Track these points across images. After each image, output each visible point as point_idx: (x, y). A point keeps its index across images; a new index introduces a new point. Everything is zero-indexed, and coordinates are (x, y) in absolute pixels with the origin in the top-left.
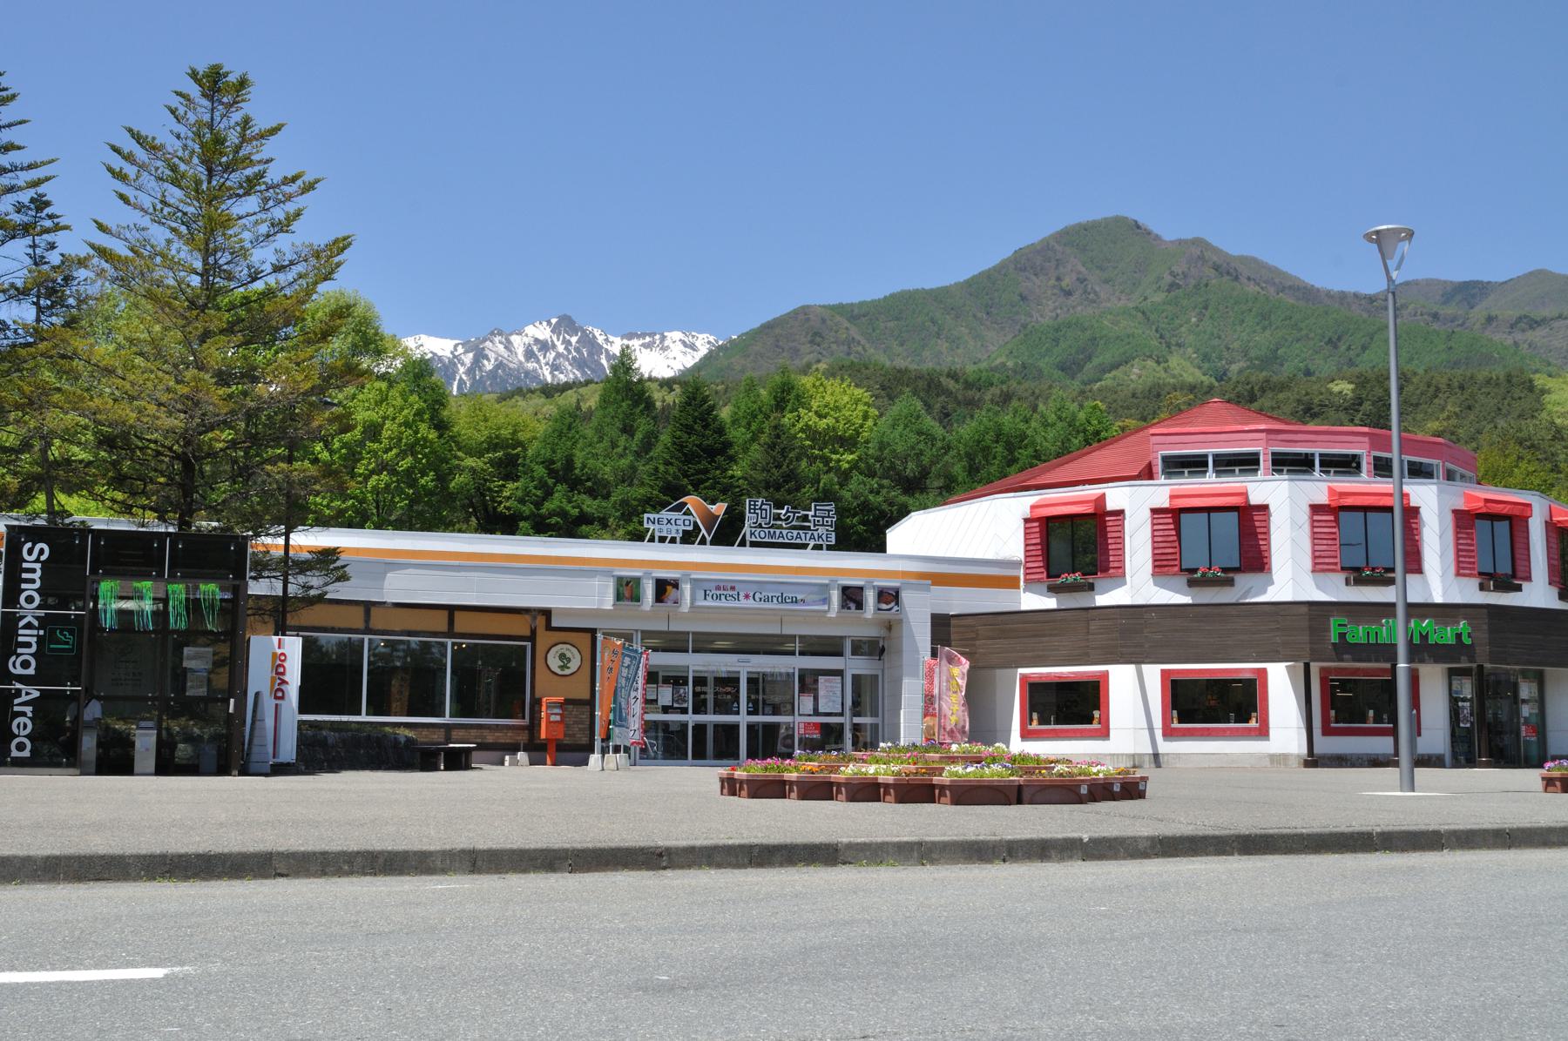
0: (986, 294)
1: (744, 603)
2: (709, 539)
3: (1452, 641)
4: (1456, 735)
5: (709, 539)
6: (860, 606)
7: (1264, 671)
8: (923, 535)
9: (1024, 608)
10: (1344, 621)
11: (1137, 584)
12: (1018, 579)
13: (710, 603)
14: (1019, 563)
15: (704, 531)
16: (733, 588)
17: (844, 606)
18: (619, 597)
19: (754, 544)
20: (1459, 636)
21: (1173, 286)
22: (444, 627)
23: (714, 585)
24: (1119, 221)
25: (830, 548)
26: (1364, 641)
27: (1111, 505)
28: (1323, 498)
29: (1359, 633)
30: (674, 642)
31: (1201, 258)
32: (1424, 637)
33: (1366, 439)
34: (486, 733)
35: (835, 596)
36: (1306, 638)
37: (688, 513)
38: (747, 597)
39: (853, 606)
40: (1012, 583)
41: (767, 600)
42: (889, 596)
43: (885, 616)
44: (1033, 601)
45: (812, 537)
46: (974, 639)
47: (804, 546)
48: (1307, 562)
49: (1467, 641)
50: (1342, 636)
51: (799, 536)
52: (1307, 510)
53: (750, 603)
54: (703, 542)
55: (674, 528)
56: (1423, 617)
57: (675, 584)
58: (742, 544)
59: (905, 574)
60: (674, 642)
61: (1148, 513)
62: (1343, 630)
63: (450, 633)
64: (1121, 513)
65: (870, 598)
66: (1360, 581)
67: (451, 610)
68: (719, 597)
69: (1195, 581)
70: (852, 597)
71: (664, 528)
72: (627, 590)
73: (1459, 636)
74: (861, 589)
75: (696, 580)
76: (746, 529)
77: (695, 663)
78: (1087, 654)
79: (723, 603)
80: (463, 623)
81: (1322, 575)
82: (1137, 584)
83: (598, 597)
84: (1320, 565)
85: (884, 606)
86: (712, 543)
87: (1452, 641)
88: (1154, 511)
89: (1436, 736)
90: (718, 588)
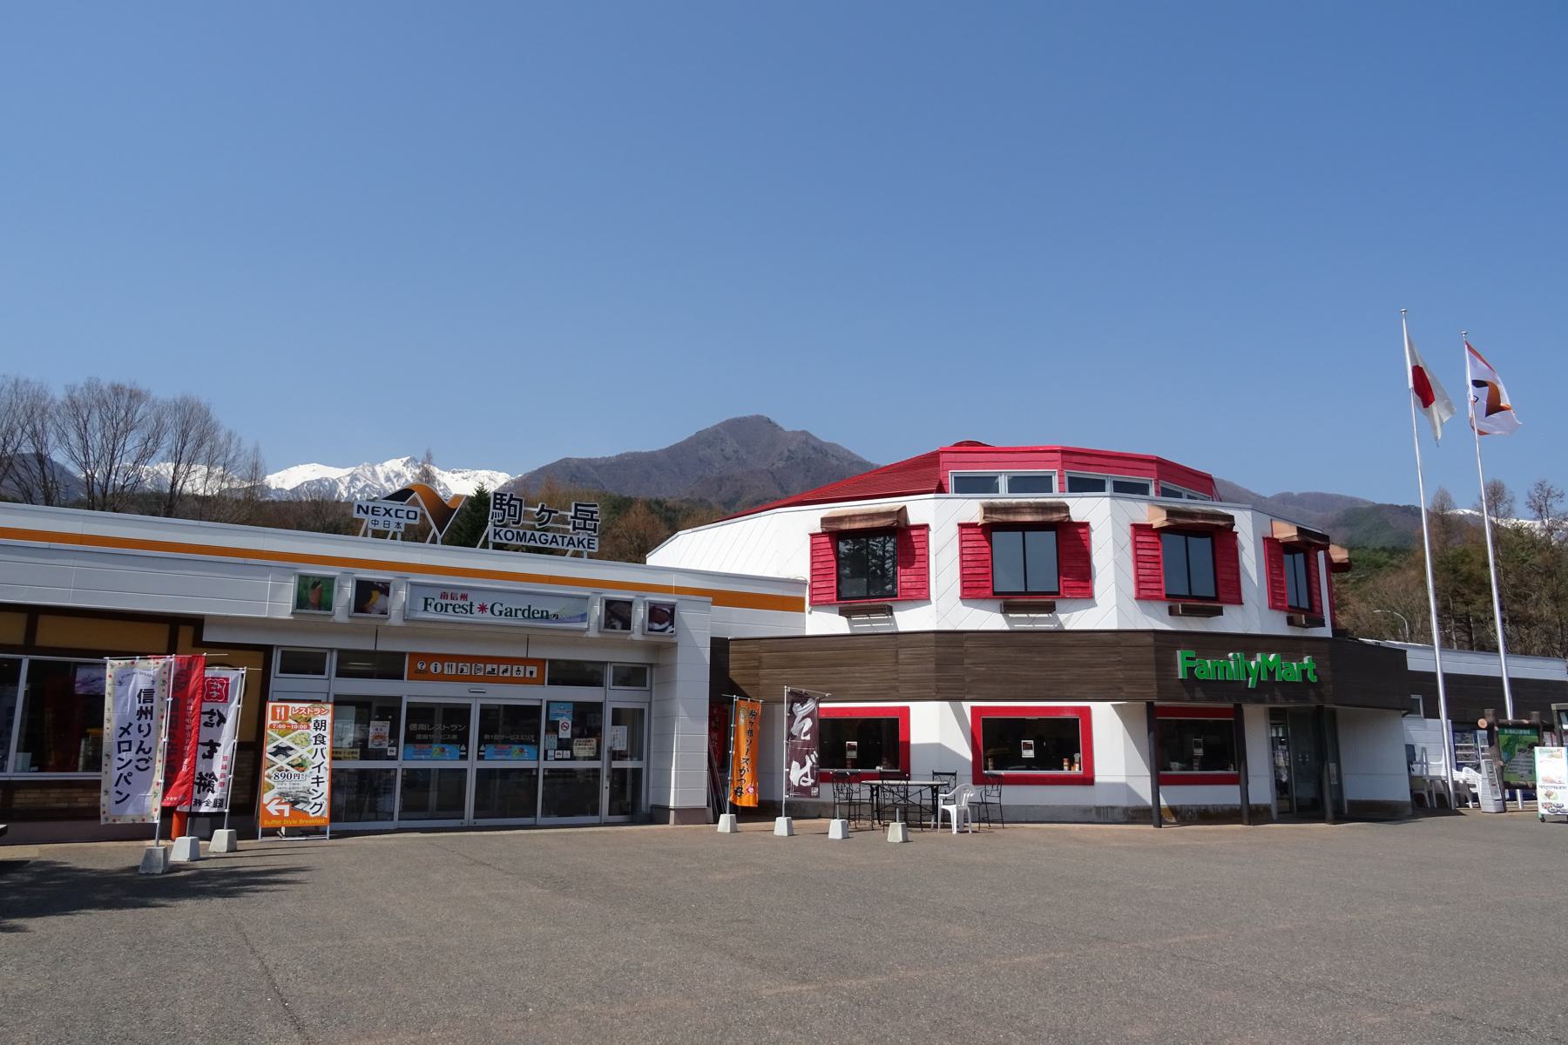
0: (676, 454)
1: (478, 617)
2: (440, 537)
3: (1299, 679)
4: (1281, 788)
5: (440, 537)
6: (627, 625)
7: (907, 709)
8: (693, 552)
9: (808, 632)
10: (1192, 654)
11: (942, 607)
12: (803, 600)
13: (431, 615)
14: (804, 583)
15: (435, 529)
16: (464, 597)
17: (609, 624)
18: (301, 603)
19: (497, 547)
20: (1304, 672)
21: (789, 458)
22: (18, 637)
23: (439, 592)
24: (759, 418)
25: (590, 556)
26: (1212, 677)
27: (914, 519)
28: (1159, 520)
29: (1207, 668)
30: (389, 666)
31: (806, 442)
32: (1271, 673)
33: (1154, 466)
34: (76, 793)
35: (597, 610)
36: (1153, 674)
37: (415, 503)
38: (483, 608)
39: (618, 624)
40: (795, 605)
41: (510, 613)
42: (662, 615)
43: (655, 638)
44: (825, 623)
45: (571, 542)
46: (757, 668)
47: (564, 553)
48: (1131, 589)
49: (1312, 678)
50: (1191, 670)
51: (554, 540)
52: (1129, 530)
53: (487, 617)
54: (434, 541)
55: (393, 520)
56: (1269, 651)
57: (384, 589)
58: (485, 545)
59: (680, 590)
60: (389, 666)
61: (956, 529)
62: (1191, 664)
63: (29, 647)
64: (926, 527)
65: (640, 614)
66: (1189, 612)
67: (33, 613)
68: (444, 608)
69: (1010, 604)
70: (617, 613)
71: (381, 519)
72: (314, 595)
73: (1304, 672)
74: (630, 603)
75: (413, 584)
76: (490, 528)
77: (410, 691)
78: (895, 688)
79: (449, 616)
80: (48, 634)
81: (1145, 603)
82: (942, 607)
83: (276, 601)
84: (1145, 592)
85: (657, 626)
86: (443, 542)
87: (1299, 679)
88: (962, 526)
89: (1261, 791)
90: (444, 596)
